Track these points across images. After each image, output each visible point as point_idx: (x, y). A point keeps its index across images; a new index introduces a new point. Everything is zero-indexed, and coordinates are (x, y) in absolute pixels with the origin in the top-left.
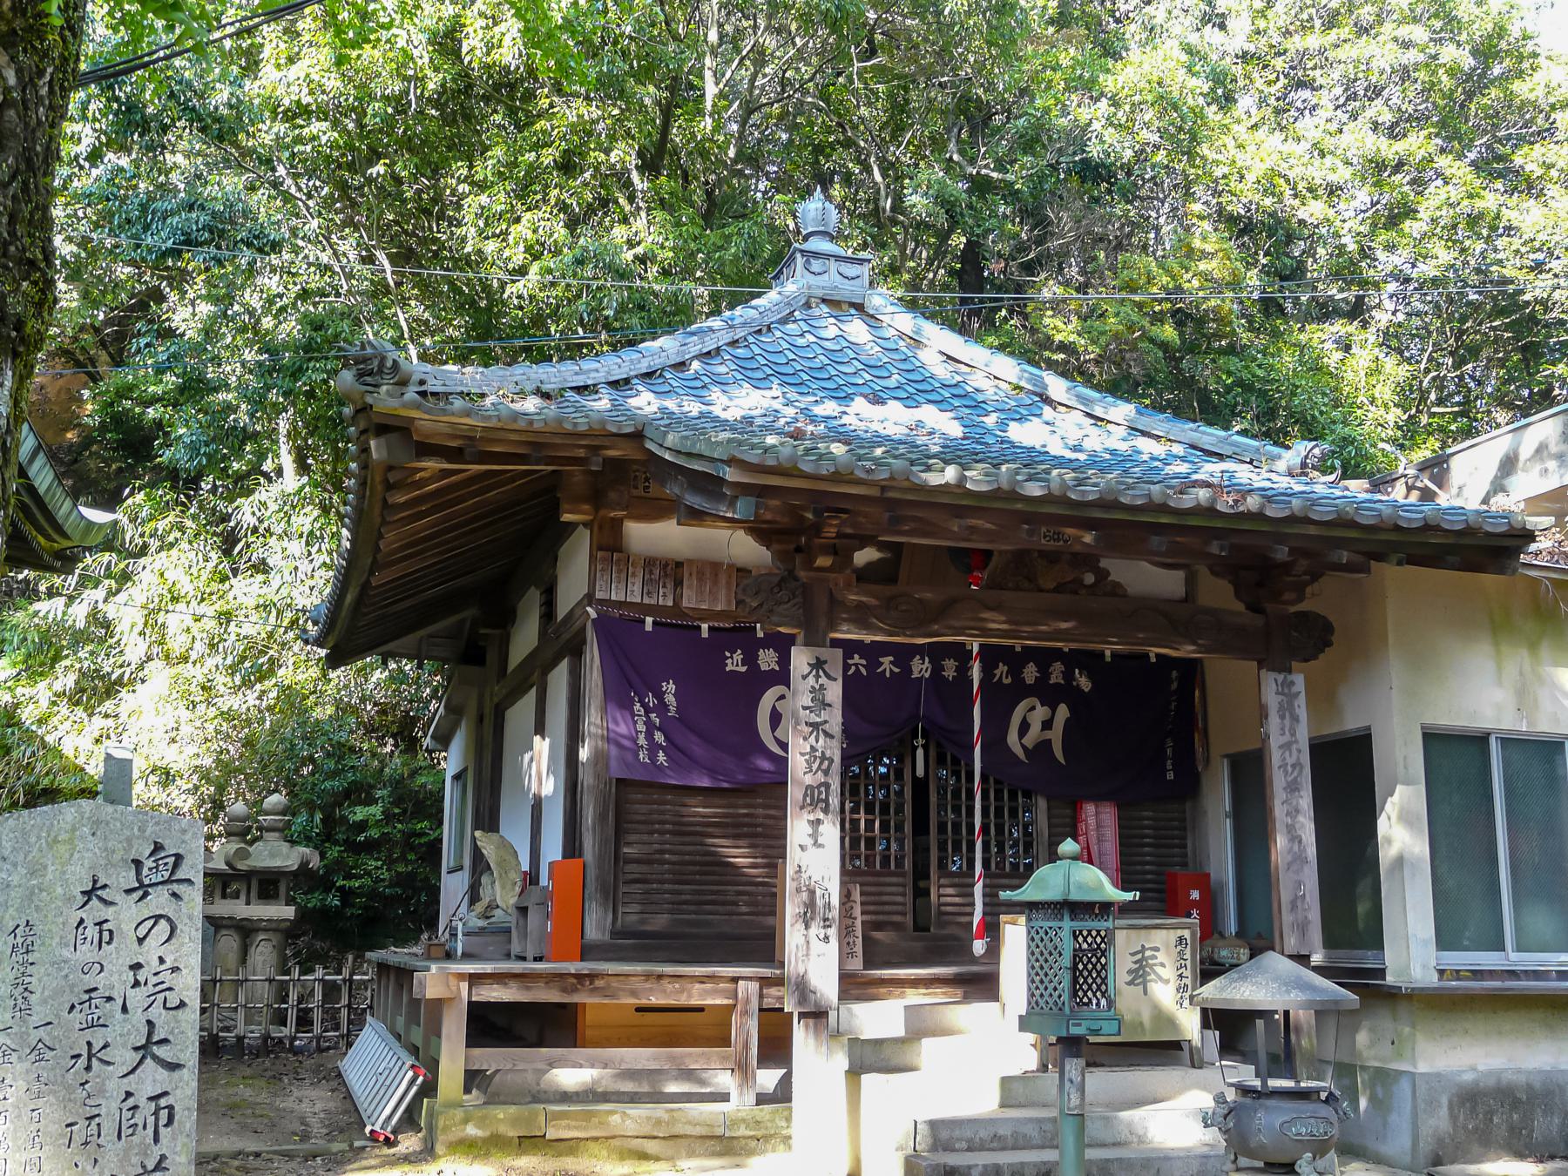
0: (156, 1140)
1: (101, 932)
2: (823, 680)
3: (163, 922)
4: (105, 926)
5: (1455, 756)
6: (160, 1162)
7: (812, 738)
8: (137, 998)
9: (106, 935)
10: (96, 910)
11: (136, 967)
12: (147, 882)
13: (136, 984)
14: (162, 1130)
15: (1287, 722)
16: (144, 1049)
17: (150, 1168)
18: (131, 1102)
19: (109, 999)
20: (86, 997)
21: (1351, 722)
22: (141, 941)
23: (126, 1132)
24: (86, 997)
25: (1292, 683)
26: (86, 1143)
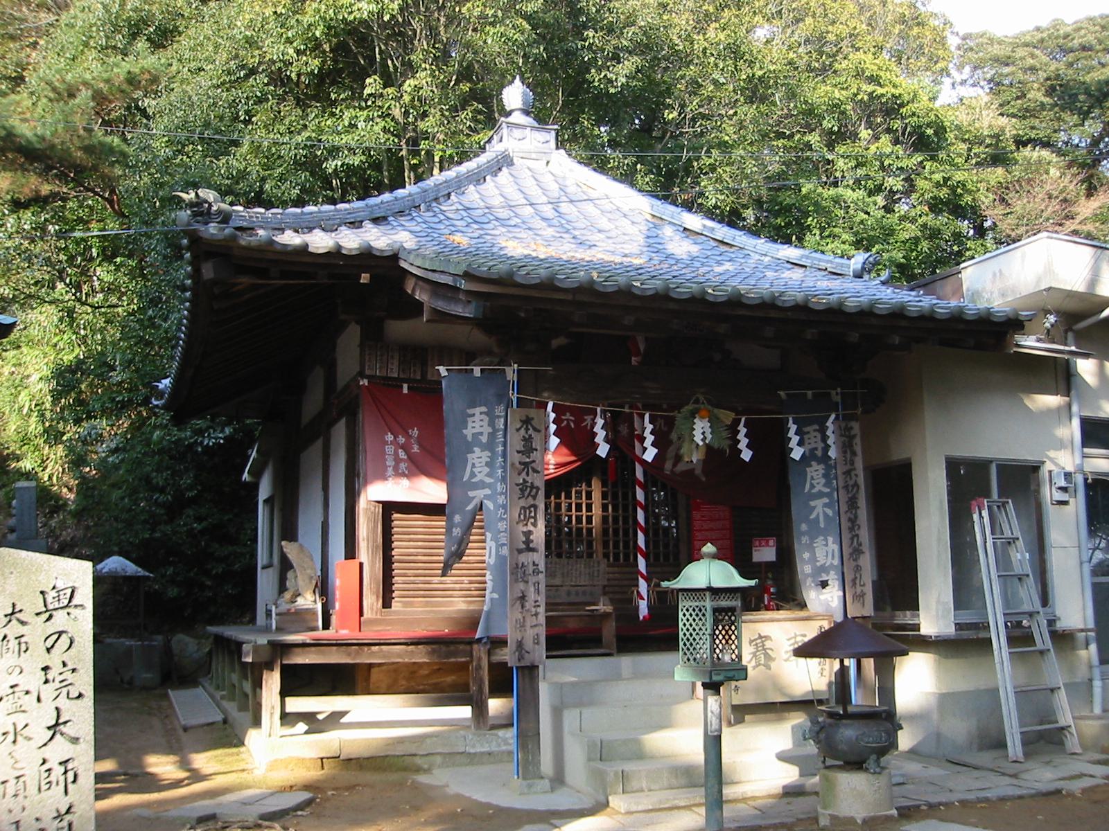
0: (66, 792)
1: (19, 644)
2: (531, 431)
3: (64, 636)
4: (23, 640)
5: (967, 480)
6: (70, 808)
7: (524, 474)
8: (48, 692)
9: (23, 647)
10: (14, 629)
11: (46, 669)
12: (51, 607)
13: (46, 682)
14: (70, 786)
15: (848, 455)
16: (54, 728)
17: (63, 812)
18: (46, 767)
19: (27, 693)
20: (11, 691)
21: (897, 455)
22: (48, 650)
23: (44, 787)
24: (11, 691)
25: (852, 428)
26: (16, 795)
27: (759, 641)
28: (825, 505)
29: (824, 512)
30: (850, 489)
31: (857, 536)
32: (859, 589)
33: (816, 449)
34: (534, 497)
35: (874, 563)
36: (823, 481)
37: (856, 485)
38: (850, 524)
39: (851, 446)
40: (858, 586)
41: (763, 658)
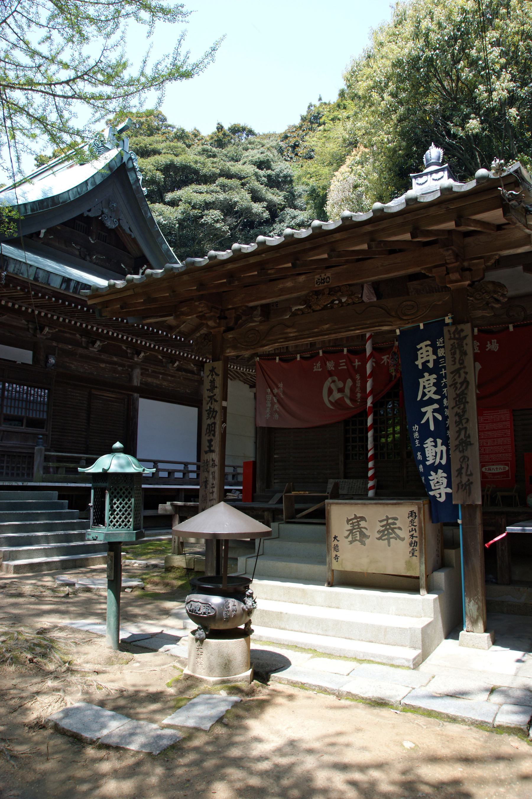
7: (209, 404)
27: (355, 521)
28: (435, 411)
29: (434, 416)
30: (458, 386)
31: (466, 428)
32: (465, 479)
33: (428, 361)
34: (214, 418)
35: (439, 609)
36: (434, 389)
37: (466, 382)
38: (457, 418)
39: (461, 346)
40: (464, 475)
41: (358, 535)
